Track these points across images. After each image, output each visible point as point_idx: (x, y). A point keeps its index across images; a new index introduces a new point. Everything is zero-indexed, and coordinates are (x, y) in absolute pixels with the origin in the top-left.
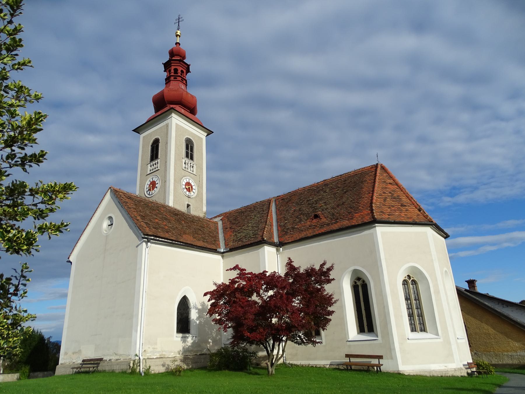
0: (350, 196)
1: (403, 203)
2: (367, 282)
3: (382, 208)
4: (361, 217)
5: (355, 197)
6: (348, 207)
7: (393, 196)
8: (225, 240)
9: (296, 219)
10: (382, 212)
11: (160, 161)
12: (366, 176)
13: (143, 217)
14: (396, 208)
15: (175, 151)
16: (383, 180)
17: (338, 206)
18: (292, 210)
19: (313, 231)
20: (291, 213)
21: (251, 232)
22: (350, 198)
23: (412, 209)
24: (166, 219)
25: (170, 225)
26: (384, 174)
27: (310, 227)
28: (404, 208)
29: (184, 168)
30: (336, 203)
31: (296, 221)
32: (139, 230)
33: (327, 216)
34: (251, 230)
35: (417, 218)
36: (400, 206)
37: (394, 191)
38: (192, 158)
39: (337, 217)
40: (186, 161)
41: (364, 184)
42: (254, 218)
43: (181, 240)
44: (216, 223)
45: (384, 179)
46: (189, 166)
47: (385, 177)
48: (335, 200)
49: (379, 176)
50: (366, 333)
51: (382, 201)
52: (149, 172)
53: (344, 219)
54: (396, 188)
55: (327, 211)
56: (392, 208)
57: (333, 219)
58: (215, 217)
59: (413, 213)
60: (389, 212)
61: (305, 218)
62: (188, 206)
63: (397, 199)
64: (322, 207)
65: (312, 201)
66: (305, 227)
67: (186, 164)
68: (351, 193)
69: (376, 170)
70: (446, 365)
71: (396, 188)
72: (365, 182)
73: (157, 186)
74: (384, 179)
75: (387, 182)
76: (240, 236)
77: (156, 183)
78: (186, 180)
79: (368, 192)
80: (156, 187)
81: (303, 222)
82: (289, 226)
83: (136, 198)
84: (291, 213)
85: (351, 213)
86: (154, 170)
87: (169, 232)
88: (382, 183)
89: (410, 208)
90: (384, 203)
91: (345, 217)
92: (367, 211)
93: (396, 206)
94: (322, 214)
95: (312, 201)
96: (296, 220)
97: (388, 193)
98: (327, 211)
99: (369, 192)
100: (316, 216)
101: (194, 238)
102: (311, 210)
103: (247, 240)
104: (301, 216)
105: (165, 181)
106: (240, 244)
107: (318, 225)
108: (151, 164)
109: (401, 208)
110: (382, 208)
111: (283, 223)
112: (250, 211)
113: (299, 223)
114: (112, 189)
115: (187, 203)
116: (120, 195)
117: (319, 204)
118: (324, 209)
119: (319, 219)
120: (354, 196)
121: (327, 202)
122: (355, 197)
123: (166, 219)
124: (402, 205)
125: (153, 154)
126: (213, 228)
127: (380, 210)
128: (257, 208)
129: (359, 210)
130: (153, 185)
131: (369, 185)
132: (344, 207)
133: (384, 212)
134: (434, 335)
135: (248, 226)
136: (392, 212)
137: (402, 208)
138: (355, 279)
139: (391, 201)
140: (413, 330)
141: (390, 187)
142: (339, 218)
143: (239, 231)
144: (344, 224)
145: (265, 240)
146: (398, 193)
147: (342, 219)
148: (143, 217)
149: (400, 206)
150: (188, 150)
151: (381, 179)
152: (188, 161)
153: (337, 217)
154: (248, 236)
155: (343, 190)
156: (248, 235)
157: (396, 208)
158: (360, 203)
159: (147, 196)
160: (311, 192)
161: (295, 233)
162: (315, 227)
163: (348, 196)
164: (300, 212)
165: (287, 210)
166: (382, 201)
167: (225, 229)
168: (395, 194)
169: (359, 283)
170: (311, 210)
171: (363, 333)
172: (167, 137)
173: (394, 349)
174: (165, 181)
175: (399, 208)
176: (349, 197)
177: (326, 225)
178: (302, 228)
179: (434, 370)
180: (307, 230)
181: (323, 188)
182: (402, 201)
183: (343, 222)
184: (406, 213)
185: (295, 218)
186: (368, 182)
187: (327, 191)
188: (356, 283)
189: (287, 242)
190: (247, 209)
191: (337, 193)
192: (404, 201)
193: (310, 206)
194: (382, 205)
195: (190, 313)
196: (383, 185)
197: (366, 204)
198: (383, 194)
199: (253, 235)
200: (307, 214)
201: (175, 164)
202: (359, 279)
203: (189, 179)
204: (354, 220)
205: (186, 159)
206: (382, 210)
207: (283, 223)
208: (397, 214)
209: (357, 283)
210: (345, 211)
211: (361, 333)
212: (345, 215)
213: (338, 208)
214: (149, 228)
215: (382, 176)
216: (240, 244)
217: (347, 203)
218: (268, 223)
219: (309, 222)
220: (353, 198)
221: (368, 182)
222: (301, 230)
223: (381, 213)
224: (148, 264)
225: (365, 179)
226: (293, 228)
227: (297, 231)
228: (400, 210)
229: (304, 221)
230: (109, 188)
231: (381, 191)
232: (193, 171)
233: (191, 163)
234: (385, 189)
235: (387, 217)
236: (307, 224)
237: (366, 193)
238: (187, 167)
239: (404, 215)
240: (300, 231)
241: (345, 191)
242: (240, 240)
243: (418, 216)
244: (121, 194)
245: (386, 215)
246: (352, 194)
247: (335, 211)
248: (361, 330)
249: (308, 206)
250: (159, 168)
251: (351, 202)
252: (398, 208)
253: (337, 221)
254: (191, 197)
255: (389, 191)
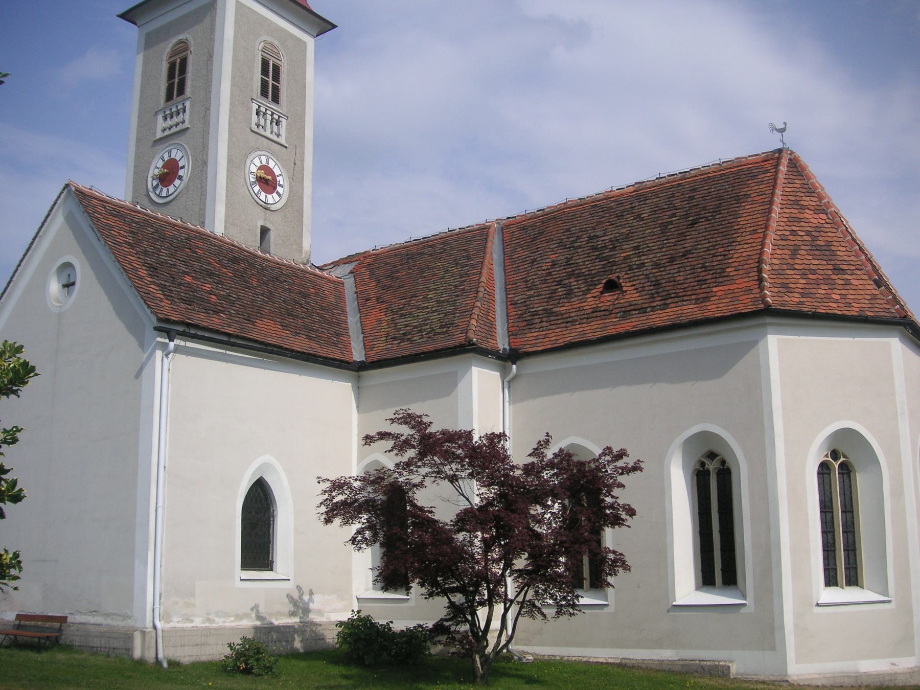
0: (705, 234)
1: (838, 263)
2: (730, 463)
3: (785, 276)
4: (729, 296)
5: (718, 239)
6: (697, 267)
7: (816, 243)
8: (363, 333)
9: (558, 287)
10: (784, 286)
11: (191, 106)
12: (750, 182)
13: (152, 269)
14: (821, 277)
15: (233, 78)
16: (793, 198)
17: (672, 260)
18: (548, 260)
19: (600, 326)
20: (544, 270)
21: (435, 316)
22: (703, 242)
23: (861, 282)
24: (210, 274)
25: (222, 293)
26: (797, 181)
27: (593, 312)
28: (840, 276)
29: (254, 128)
30: (666, 253)
31: (558, 294)
32: (146, 307)
33: (641, 285)
34: (436, 311)
35: (870, 306)
36: (830, 272)
37: (818, 229)
38: (276, 99)
39: (666, 293)
40: (259, 107)
41: (743, 204)
42: (443, 278)
43: (253, 335)
44: (339, 284)
45: (796, 194)
46: (268, 122)
47: (798, 190)
48: (665, 242)
49: (784, 185)
50: (719, 588)
51: (787, 257)
52: (159, 135)
53: (685, 298)
54: (824, 222)
55: (641, 273)
56: (811, 276)
57: (656, 295)
58: (336, 264)
59: (861, 292)
60: (803, 286)
61: (581, 286)
62: (264, 231)
63: (824, 252)
64: (628, 261)
65: (602, 239)
66: (579, 313)
67: (261, 116)
68: (707, 226)
69: (777, 166)
70: (894, 660)
71: (824, 222)
72: (745, 200)
73: (181, 172)
74: (796, 194)
75: (802, 203)
76: (407, 326)
77: (180, 165)
78: (260, 159)
79: (752, 229)
80: (180, 178)
81: (576, 298)
82: (537, 305)
83: (133, 214)
84: (544, 270)
85: (703, 282)
86: (174, 130)
87: (223, 312)
88: (790, 207)
89: (854, 276)
90: (791, 261)
91: (689, 293)
92: (749, 281)
93: (822, 272)
94: (628, 280)
95: (602, 239)
96: (555, 292)
97: (803, 233)
98: (641, 273)
99: (755, 228)
100: (612, 286)
101: (285, 327)
102: (599, 265)
103: (425, 339)
104: (571, 280)
105: (205, 163)
106: (405, 349)
107: (617, 311)
108: (166, 113)
109: (833, 277)
110: (785, 276)
111: (521, 297)
112: (431, 255)
113: (565, 300)
114: (74, 189)
115: (260, 223)
116: (95, 206)
117: (621, 251)
118: (635, 267)
119: (619, 294)
120: (715, 236)
121: (643, 248)
122: (718, 239)
123: (210, 274)
124: (837, 270)
125: (173, 83)
126: (332, 299)
127: (781, 281)
128: (452, 248)
129: (726, 276)
130: (169, 174)
131: (756, 209)
132: (688, 264)
133: (791, 286)
134: (877, 593)
135: (426, 299)
136: (810, 286)
137: (836, 277)
138: (702, 457)
139: (810, 257)
140: (831, 580)
141: (809, 217)
142: (673, 295)
143: (401, 309)
144: (685, 311)
145: (474, 344)
146: (830, 234)
147: (681, 299)
148: (153, 270)
149: (830, 272)
150: (267, 76)
151: (788, 194)
152: (268, 103)
153: (666, 293)
154: (428, 327)
155: (687, 216)
156: (427, 324)
157: (821, 277)
158: (729, 256)
159: (153, 199)
160: (600, 214)
161: (554, 327)
162: (607, 313)
163: (701, 235)
164: (567, 270)
165: (534, 260)
166: (787, 257)
167: (363, 300)
168: (820, 238)
169: (712, 466)
170: (599, 265)
171: (711, 588)
172: (212, 40)
173: (782, 627)
174: (202, 164)
175: (828, 277)
176: (703, 238)
177: (637, 312)
178: (573, 314)
179: (865, 673)
180: (584, 321)
181: (633, 205)
182: (837, 257)
183: (684, 308)
184: (844, 292)
185: (554, 284)
186: (755, 199)
187: (643, 216)
188: (703, 464)
189: (530, 350)
190: (424, 247)
191: (671, 223)
192: (841, 258)
193: (595, 254)
194: (785, 267)
195: (274, 521)
196: (792, 210)
197: (745, 262)
198: (791, 237)
199: (442, 327)
200: (587, 277)
201: (232, 114)
202: (712, 455)
203: (268, 158)
204: (712, 303)
205: (262, 100)
206: (785, 281)
207: (521, 297)
208: (823, 292)
209: (707, 466)
210: (689, 276)
211: (706, 588)
212: (689, 287)
213: (672, 267)
214: (170, 302)
215: (792, 186)
216: (406, 349)
217: (695, 255)
218: (481, 295)
219: (593, 299)
220: (711, 240)
221: (755, 199)
222: (568, 320)
223: (781, 290)
224: (169, 397)
225: (746, 190)
226: (549, 313)
227: (559, 322)
228: (831, 281)
229: (579, 294)
230: (63, 186)
231: (787, 228)
232: (278, 136)
233: (273, 113)
234: (795, 224)
235: (797, 300)
236: (586, 304)
237: (747, 230)
238: (262, 122)
239: (838, 297)
240: (567, 322)
241: (691, 218)
242: (404, 337)
243: (873, 301)
244: (95, 202)
245: (796, 295)
246: (710, 229)
247: (663, 273)
248: (706, 579)
249: (592, 254)
250: (187, 125)
251: (708, 253)
252: (825, 277)
253: (667, 302)
254: (273, 207)
255: (806, 229)
